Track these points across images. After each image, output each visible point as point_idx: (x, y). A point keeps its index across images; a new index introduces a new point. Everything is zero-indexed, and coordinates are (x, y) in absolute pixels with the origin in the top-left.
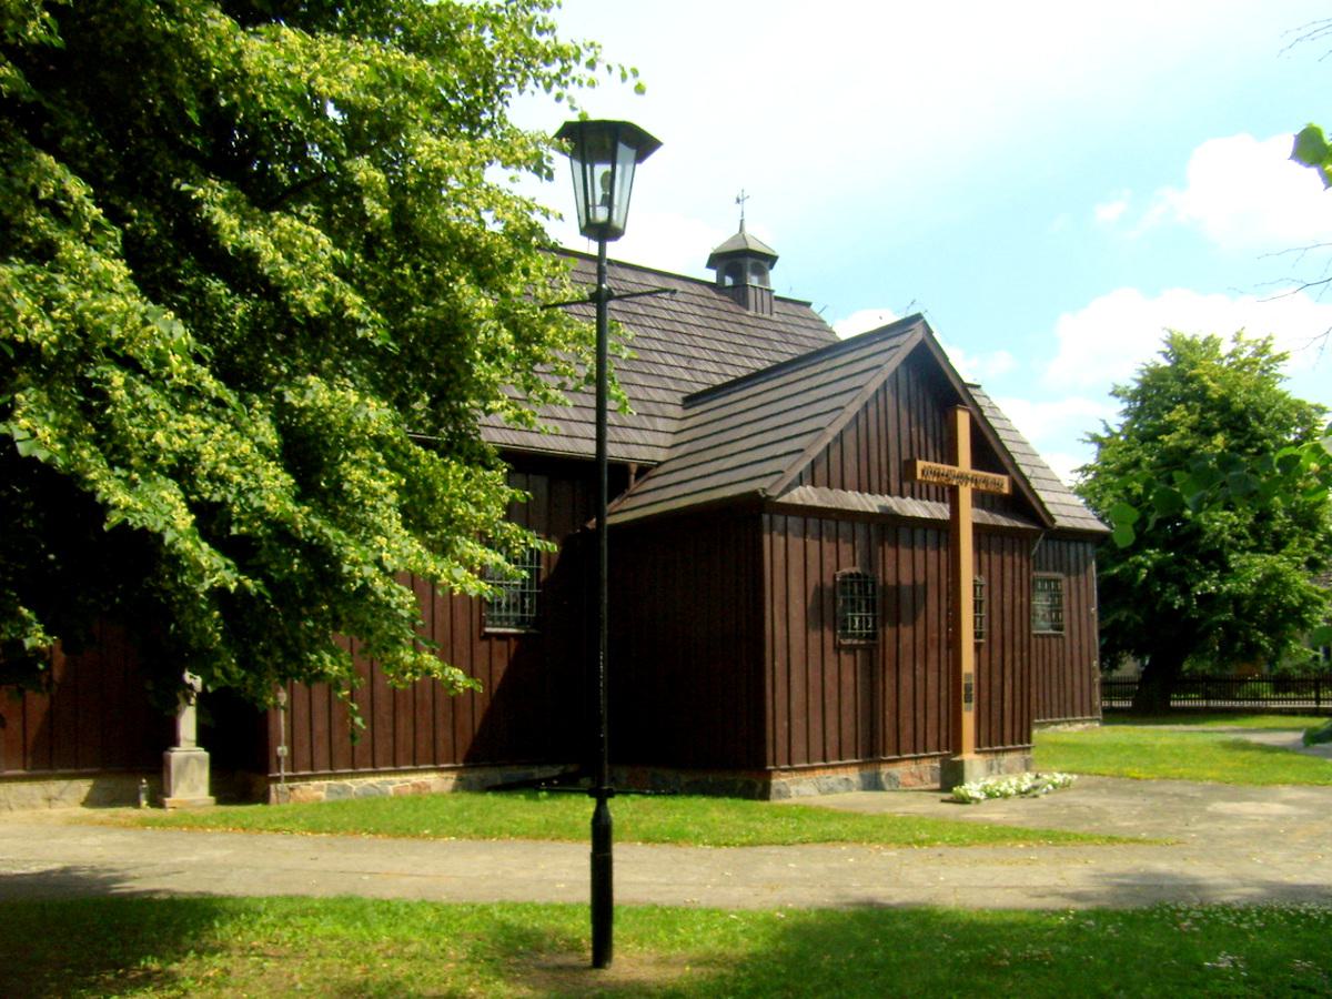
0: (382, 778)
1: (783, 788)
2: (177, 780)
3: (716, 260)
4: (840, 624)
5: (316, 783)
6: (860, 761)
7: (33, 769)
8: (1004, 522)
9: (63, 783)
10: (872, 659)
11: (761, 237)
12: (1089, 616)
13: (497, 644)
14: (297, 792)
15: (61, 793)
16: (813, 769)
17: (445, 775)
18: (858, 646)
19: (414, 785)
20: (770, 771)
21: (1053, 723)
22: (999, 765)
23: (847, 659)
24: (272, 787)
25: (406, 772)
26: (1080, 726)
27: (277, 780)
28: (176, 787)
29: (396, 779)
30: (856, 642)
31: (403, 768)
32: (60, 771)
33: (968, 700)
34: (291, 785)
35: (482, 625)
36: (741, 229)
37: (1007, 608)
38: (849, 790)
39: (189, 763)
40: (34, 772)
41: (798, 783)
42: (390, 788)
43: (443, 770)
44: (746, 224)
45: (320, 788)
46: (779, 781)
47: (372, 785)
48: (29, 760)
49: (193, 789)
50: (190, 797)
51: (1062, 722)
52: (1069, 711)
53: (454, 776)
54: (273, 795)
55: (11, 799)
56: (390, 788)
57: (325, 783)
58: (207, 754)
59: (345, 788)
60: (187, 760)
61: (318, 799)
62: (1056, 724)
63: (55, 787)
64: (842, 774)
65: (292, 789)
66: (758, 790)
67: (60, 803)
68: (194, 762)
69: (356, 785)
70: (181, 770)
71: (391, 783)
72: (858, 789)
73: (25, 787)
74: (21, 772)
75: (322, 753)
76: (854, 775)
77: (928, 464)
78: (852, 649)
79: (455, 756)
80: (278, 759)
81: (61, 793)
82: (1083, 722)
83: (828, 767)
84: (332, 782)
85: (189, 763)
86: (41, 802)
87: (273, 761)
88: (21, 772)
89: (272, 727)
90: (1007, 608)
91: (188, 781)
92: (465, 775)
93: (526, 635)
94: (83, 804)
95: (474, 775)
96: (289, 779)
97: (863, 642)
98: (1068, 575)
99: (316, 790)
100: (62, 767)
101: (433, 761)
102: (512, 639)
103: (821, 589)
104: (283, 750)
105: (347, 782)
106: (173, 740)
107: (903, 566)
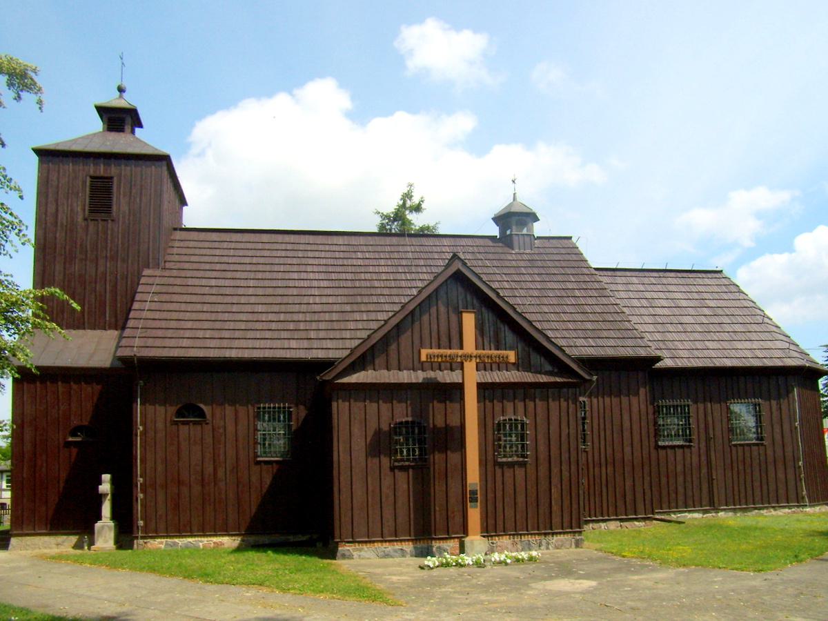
0: (196, 539)
1: (347, 553)
2: (98, 537)
3: (498, 219)
4: (392, 452)
5: (159, 540)
6: (413, 538)
7: (51, 530)
8: (558, 380)
9: (65, 537)
10: (421, 472)
11: (529, 199)
12: (793, 430)
13: (264, 467)
14: (149, 544)
15: (63, 542)
16: (374, 542)
17: (234, 538)
18: (409, 467)
19: (214, 543)
20: (337, 543)
21: (756, 508)
22: (548, 544)
23: (401, 476)
24: (135, 541)
25: (210, 536)
26: (787, 510)
27: (137, 538)
28: (98, 540)
29: (205, 540)
30: (407, 463)
31: (208, 533)
32: (62, 531)
33: (474, 500)
34: (145, 541)
35: (657, 434)
36: (514, 199)
37: (554, 437)
38: (403, 556)
39: (105, 527)
40: (51, 532)
41: (360, 550)
42: (201, 544)
43: (232, 535)
44: (517, 195)
45: (162, 543)
46: (343, 548)
47: (190, 542)
48: (49, 526)
49: (106, 541)
50: (105, 545)
51: (767, 508)
52: (743, 501)
53: (239, 539)
54: (135, 546)
55: (40, 544)
56: (201, 544)
57: (164, 540)
58: (113, 524)
59: (175, 544)
60: (103, 527)
61: (160, 548)
62: (760, 509)
63: (60, 539)
64: (398, 546)
65: (145, 543)
66: (331, 553)
67: (62, 547)
68: (106, 529)
69: (181, 542)
70: (100, 532)
71: (201, 542)
72: (411, 556)
73: (46, 538)
74: (44, 531)
75: (162, 526)
76: (408, 547)
77: (430, 351)
78: (402, 468)
79: (239, 528)
80: (138, 527)
81: (63, 542)
82: (790, 507)
83: (386, 541)
84: (168, 540)
85: (105, 527)
86: (54, 546)
87: (135, 528)
88: (44, 531)
89: (135, 511)
90: (554, 437)
91: (103, 538)
92: (245, 539)
93: (283, 461)
94: (73, 548)
95: (252, 539)
96: (143, 538)
97: (412, 464)
98: (696, 402)
99: (159, 544)
100: (63, 530)
101: (225, 530)
102: (274, 464)
103: (378, 432)
104: (141, 523)
105: (177, 540)
106: (99, 518)
107: (438, 415)
